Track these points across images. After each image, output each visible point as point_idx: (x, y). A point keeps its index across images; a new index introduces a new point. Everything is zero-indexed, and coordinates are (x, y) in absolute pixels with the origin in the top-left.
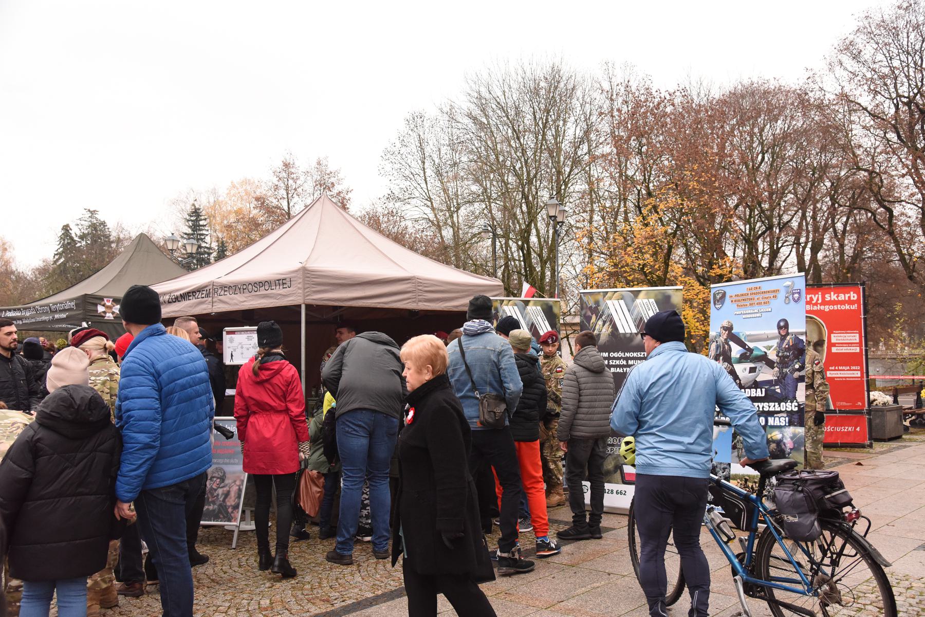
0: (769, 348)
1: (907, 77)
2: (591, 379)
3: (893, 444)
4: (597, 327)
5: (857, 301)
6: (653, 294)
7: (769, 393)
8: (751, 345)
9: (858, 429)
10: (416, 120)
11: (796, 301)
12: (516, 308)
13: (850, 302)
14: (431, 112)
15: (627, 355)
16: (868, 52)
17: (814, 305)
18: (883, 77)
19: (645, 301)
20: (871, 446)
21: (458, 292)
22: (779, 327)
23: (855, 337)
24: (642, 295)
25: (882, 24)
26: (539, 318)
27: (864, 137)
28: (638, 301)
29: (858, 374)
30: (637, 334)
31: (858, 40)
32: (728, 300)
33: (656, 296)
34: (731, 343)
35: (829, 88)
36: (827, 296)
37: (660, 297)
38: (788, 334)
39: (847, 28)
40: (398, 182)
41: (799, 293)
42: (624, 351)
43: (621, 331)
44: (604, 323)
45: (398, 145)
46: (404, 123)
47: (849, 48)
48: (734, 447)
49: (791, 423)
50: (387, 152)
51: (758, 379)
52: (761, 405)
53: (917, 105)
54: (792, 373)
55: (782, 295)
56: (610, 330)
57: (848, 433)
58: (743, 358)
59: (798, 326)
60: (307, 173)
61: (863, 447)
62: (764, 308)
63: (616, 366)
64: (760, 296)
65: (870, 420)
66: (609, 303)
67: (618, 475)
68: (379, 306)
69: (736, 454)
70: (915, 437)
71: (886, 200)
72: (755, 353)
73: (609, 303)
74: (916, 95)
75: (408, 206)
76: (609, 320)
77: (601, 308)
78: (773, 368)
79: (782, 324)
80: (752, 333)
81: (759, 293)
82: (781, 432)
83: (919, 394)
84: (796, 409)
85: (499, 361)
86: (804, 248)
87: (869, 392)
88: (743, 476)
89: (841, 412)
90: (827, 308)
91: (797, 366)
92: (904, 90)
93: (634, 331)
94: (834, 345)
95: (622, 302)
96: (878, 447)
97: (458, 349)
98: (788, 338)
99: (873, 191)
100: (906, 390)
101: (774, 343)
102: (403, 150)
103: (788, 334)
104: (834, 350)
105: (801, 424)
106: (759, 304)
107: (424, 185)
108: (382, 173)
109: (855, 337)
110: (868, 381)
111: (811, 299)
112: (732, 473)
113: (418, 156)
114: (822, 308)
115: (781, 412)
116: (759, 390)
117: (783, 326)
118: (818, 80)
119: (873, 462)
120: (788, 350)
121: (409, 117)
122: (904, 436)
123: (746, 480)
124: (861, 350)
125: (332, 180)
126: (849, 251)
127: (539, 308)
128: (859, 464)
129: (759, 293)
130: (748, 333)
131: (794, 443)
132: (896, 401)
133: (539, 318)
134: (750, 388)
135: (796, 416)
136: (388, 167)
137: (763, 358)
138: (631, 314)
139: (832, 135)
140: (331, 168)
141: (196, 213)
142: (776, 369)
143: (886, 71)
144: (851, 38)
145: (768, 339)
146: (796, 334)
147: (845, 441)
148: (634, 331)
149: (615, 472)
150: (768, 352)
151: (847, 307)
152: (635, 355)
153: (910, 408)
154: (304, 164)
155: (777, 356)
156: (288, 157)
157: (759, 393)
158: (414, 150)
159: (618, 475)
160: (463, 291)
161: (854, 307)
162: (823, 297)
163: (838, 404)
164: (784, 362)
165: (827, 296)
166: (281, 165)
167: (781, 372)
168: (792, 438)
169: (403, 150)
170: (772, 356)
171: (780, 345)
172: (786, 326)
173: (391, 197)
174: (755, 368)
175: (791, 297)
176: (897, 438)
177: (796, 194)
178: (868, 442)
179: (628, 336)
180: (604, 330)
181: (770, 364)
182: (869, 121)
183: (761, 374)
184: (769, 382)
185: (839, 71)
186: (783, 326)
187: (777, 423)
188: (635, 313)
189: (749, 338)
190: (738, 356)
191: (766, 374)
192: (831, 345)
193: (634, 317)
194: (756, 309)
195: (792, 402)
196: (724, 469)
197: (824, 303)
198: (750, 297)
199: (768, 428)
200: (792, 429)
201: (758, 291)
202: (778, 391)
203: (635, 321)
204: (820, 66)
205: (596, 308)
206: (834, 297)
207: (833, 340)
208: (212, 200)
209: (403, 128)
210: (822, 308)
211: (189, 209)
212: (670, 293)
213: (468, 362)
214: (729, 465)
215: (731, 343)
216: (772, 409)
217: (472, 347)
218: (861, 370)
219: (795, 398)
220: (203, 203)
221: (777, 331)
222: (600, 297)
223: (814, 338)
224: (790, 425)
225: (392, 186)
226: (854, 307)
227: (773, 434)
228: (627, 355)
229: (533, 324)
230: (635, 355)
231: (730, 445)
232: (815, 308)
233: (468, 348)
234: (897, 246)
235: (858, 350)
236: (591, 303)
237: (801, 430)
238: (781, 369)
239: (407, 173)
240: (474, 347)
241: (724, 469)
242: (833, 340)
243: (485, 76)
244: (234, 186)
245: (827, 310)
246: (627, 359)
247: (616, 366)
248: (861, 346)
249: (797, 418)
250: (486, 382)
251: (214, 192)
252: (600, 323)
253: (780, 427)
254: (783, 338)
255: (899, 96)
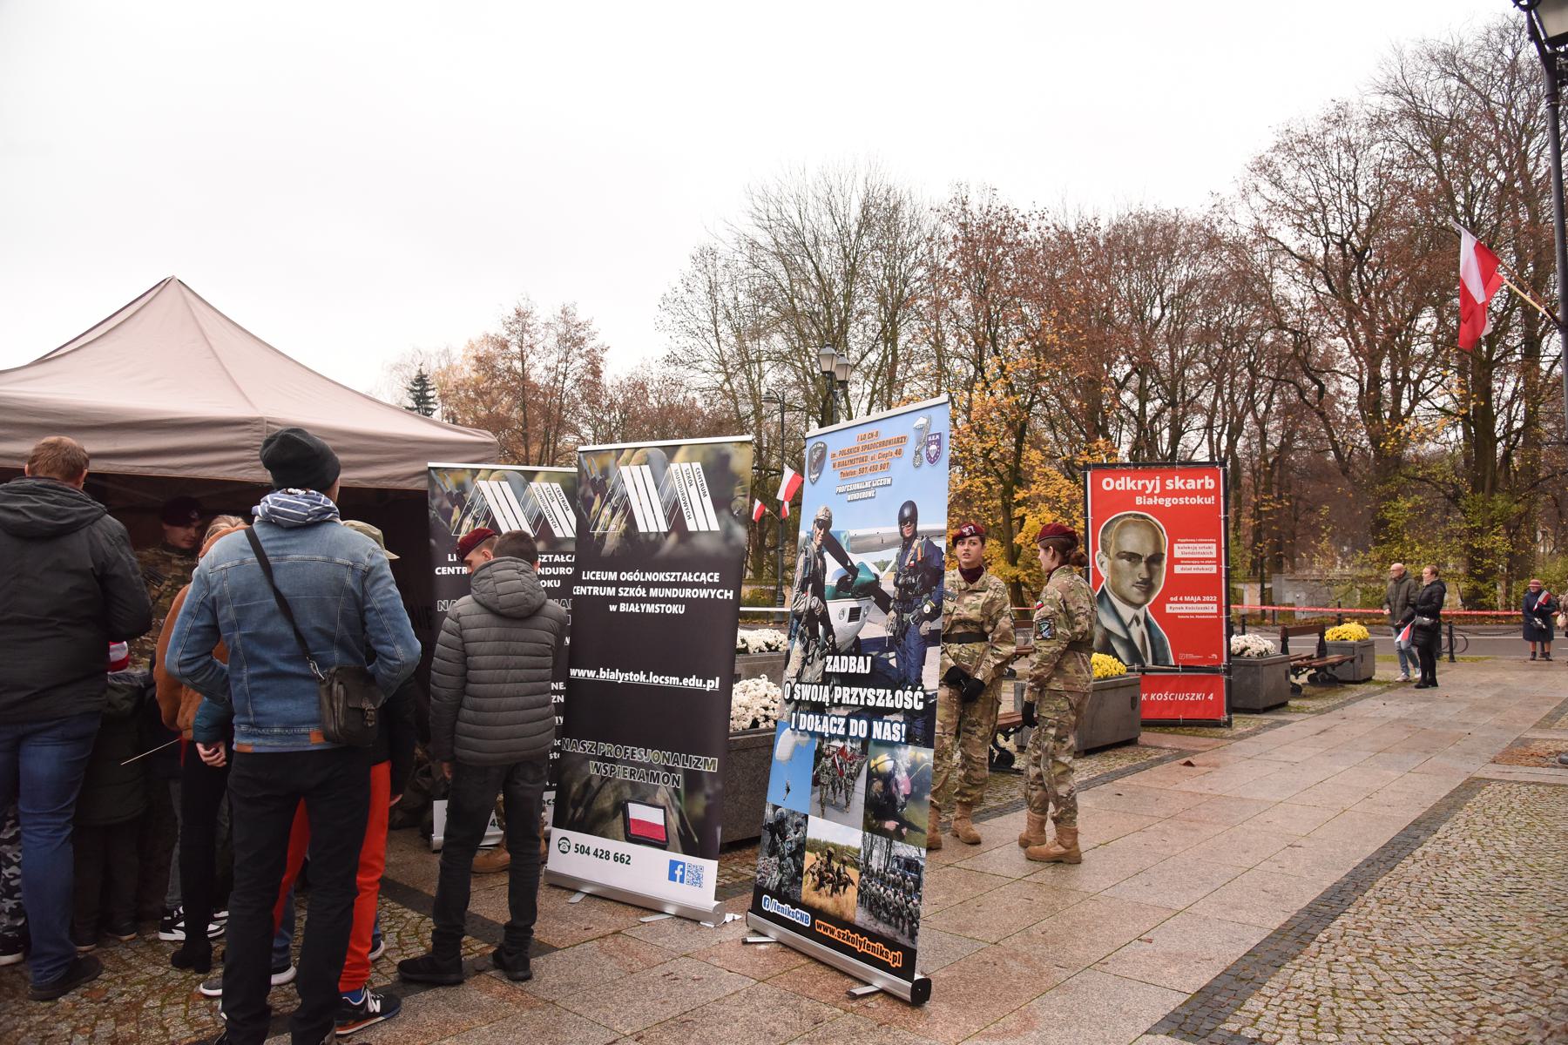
0: (883, 566)
1: (1340, 211)
2: (494, 631)
3: (1267, 719)
4: (602, 520)
5: (1215, 491)
6: (699, 454)
7: (878, 665)
8: (856, 559)
9: (1211, 697)
10: (706, 256)
11: (933, 460)
12: (505, 485)
13: (1204, 493)
14: (725, 249)
15: (649, 577)
16: (1289, 174)
17: (1149, 496)
18: (1312, 209)
19: (686, 466)
20: (1229, 724)
21: (379, 452)
22: (903, 521)
23: (1209, 549)
24: (680, 454)
25: (1306, 140)
26: (555, 505)
27: (1291, 289)
28: (674, 467)
29: (1214, 609)
30: (667, 534)
31: (1277, 160)
32: (828, 461)
33: (705, 455)
34: (827, 555)
35: (1240, 221)
36: (1169, 482)
37: (711, 458)
38: (915, 535)
39: (1264, 143)
40: (681, 339)
41: (938, 442)
42: (644, 570)
43: (642, 528)
44: (614, 511)
45: (681, 289)
46: (690, 260)
47: (1263, 166)
48: (816, 781)
49: (910, 739)
50: (664, 299)
51: (862, 636)
52: (863, 692)
53: (1352, 246)
54: (918, 624)
55: (910, 448)
56: (623, 526)
57: (1197, 702)
58: (846, 588)
59: (933, 519)
60: (548, 325)
61: (1217, 725)
62: (881, 478)
63: (629, 600)
64: (875, 452)
65: (1229, 682)
66: (624, 470)
67: (618, 823)
68: (155, 473)
69: (817, 795)
70: (1308, 703)
71: (1318, 371)
72: (862, 576)
73: (624, 470)
74: (1350, 235)
75: (692, 372)
76: (622, 505)
77: (611, 482)
78: (887, 611)
79: (907, 512)
80: (861, 532)
81: (874, 446)
82: (893, 758)
83: (1322, 635)
84: (920, 707)
85: (364, 592)
86: (1220, 435)
87: (1230, 634)
88: (826, 845)
89: (1186, 668)
90: (1168, 502)
91: (927, 609)
92: (1335, 227)
93: (664, 528)
94: (1178, 561)
95: (646, 468)
96: (1241, 724)
97: (251, 558)
98: (916, 543)
99: (1300, 363)
100: (1304, 629)
101: (891, 555)
102: (688, 297)
103: (915, 535)
104: (1178, 569)
105: (928, 742)
106: (874, 468)
107: (715, 344)
108: (659, 327)
109: (1209, 549)
110: (1228, 620)
111: (1145, 487)
112: (810, 835)
113: (708, 305)
114: (1161, 501)
115: (894, 711)
116: (861, 659)
117: (908, 517)
118: (1228, 209)
119: (1211, 757)
120: (914, 570)
121: (696, 253)
122: (1291, 703)
123: (830, 856)
124: (1219, 569)
125: (582, 334)
126: (1275, 439)
127: (557, 486)
128: (1189, 764)
129: (874, 446)
130: (852, 533)
131: (913, 784)
132: (1285, 649)
133: (555, 505)
134: (848, 654)
135: (919, 723)
136: (668, 319)
137: (871, 589)
138: (661, 494)
139: (1247, 284)
140: (581, 317)
141: (421, 380)
142: (892, 614)
143: (1312, 201)
144: (1269, 156)
145: (884, 546)
146: (930, 535)
147: (1188, 716)
148: (664, 528)
149: (615, 815)
150: (882, 575)
151: (1199, 500)
152: (661, 577)
153: (1310, 658)
154: (545, 312)
155: (896, 584)
156: (524, 304)
157: (860, 666)
158: (703, 298)
159: (618, 823)
160: (388, 451)
161: (1210, 501)
162: (1163, 485)
163: (1182, 656)
164: (906, 599)
165: (1169, 482)
166: (513, 316)
167: (900, 621)
168: (909, 772)
169: (688, 297)
170: (888, 586)
171: (901, 559)
172: (913, 519)
173: (672, 360)
174: (859, 609)
175: (924, 453)
176: (1280, 706)
177: (1208, 362)
178: (1225, 718)
179: (652, 537)
180: (613, 526)
181: (883, 602)
182: (1293, 263)
183: (867, 625)
184: (877, 643)
185: (1256, 200)
186: (908, 517)
187: (887, 736)
188: (667, 491)
189: (853, 544)
190: (835, 583)
191: (876, 626)
192: (1174, 561)
193: (664, 499)
194: (869, 479)
195: (914, 690)
196: (798, 825)
197: (1165, 493)
198: (861, 454)
199: (871, 746)
200: (908, 754)
201: (875, 441)
202: (893, 662)
203: (665, 508)
204: (1230, 191)
205: (603, 482)
206: (1179, 484)
207: (1177, 554)
208: (444, 365)
209: (688, 267)
210: (1161, 501)
211: (414, 374)
212: (730, 448)
213: (284, 590)
214: (806, 817)
215: (827, 555)
216: (880, 704)
217: (294, 556)
218: (1219, 603)
219: (919, 681)
220: (432, 368)
221: (897, 529)
222: (610, 460)
223: (1148, 551)
224: (907, 743)
225: (674, 345)
226: (1210, 501)
227: (879, 759)
228: (649, 577)
229: (540, 516)
230: (661, 577)
231: (810, 774)
232: (1150, 502)
233: (281, 558)
234: (1329, 431)
235: (1214, 571)
236: (595, 473)
237: (926, 755)
238: (900, 613)
239: (693, 326)
240: (298, 554)
241: (798, 825)
242: (1177, 554)
243: (774, 191)
244: (472, 346)
245: (1168, 504)
246: (647, 585)
247: (629, 600)
248: (1219, 564)
249: (920, 728)
250: (330, 638)
251: (446, 353)
252: (607, 511)
253: (890, 745)
254: (907, 543)
255: (1328, 233)
